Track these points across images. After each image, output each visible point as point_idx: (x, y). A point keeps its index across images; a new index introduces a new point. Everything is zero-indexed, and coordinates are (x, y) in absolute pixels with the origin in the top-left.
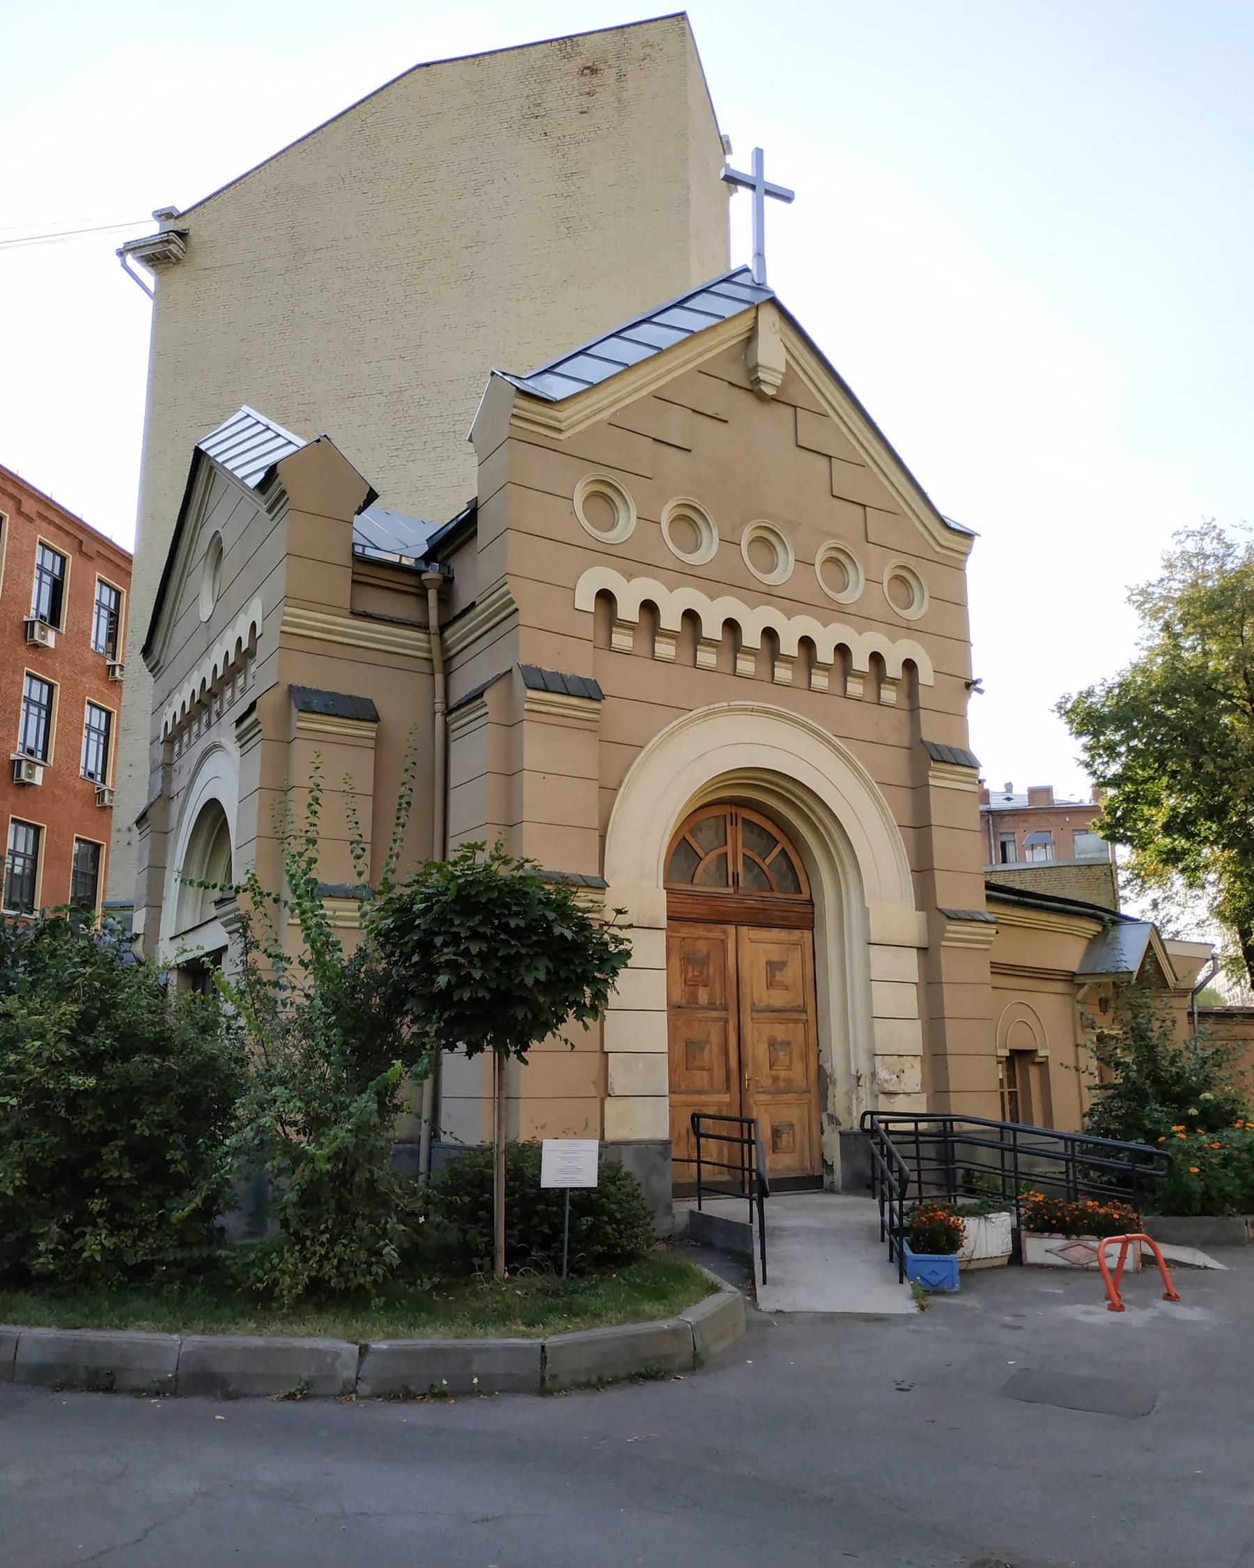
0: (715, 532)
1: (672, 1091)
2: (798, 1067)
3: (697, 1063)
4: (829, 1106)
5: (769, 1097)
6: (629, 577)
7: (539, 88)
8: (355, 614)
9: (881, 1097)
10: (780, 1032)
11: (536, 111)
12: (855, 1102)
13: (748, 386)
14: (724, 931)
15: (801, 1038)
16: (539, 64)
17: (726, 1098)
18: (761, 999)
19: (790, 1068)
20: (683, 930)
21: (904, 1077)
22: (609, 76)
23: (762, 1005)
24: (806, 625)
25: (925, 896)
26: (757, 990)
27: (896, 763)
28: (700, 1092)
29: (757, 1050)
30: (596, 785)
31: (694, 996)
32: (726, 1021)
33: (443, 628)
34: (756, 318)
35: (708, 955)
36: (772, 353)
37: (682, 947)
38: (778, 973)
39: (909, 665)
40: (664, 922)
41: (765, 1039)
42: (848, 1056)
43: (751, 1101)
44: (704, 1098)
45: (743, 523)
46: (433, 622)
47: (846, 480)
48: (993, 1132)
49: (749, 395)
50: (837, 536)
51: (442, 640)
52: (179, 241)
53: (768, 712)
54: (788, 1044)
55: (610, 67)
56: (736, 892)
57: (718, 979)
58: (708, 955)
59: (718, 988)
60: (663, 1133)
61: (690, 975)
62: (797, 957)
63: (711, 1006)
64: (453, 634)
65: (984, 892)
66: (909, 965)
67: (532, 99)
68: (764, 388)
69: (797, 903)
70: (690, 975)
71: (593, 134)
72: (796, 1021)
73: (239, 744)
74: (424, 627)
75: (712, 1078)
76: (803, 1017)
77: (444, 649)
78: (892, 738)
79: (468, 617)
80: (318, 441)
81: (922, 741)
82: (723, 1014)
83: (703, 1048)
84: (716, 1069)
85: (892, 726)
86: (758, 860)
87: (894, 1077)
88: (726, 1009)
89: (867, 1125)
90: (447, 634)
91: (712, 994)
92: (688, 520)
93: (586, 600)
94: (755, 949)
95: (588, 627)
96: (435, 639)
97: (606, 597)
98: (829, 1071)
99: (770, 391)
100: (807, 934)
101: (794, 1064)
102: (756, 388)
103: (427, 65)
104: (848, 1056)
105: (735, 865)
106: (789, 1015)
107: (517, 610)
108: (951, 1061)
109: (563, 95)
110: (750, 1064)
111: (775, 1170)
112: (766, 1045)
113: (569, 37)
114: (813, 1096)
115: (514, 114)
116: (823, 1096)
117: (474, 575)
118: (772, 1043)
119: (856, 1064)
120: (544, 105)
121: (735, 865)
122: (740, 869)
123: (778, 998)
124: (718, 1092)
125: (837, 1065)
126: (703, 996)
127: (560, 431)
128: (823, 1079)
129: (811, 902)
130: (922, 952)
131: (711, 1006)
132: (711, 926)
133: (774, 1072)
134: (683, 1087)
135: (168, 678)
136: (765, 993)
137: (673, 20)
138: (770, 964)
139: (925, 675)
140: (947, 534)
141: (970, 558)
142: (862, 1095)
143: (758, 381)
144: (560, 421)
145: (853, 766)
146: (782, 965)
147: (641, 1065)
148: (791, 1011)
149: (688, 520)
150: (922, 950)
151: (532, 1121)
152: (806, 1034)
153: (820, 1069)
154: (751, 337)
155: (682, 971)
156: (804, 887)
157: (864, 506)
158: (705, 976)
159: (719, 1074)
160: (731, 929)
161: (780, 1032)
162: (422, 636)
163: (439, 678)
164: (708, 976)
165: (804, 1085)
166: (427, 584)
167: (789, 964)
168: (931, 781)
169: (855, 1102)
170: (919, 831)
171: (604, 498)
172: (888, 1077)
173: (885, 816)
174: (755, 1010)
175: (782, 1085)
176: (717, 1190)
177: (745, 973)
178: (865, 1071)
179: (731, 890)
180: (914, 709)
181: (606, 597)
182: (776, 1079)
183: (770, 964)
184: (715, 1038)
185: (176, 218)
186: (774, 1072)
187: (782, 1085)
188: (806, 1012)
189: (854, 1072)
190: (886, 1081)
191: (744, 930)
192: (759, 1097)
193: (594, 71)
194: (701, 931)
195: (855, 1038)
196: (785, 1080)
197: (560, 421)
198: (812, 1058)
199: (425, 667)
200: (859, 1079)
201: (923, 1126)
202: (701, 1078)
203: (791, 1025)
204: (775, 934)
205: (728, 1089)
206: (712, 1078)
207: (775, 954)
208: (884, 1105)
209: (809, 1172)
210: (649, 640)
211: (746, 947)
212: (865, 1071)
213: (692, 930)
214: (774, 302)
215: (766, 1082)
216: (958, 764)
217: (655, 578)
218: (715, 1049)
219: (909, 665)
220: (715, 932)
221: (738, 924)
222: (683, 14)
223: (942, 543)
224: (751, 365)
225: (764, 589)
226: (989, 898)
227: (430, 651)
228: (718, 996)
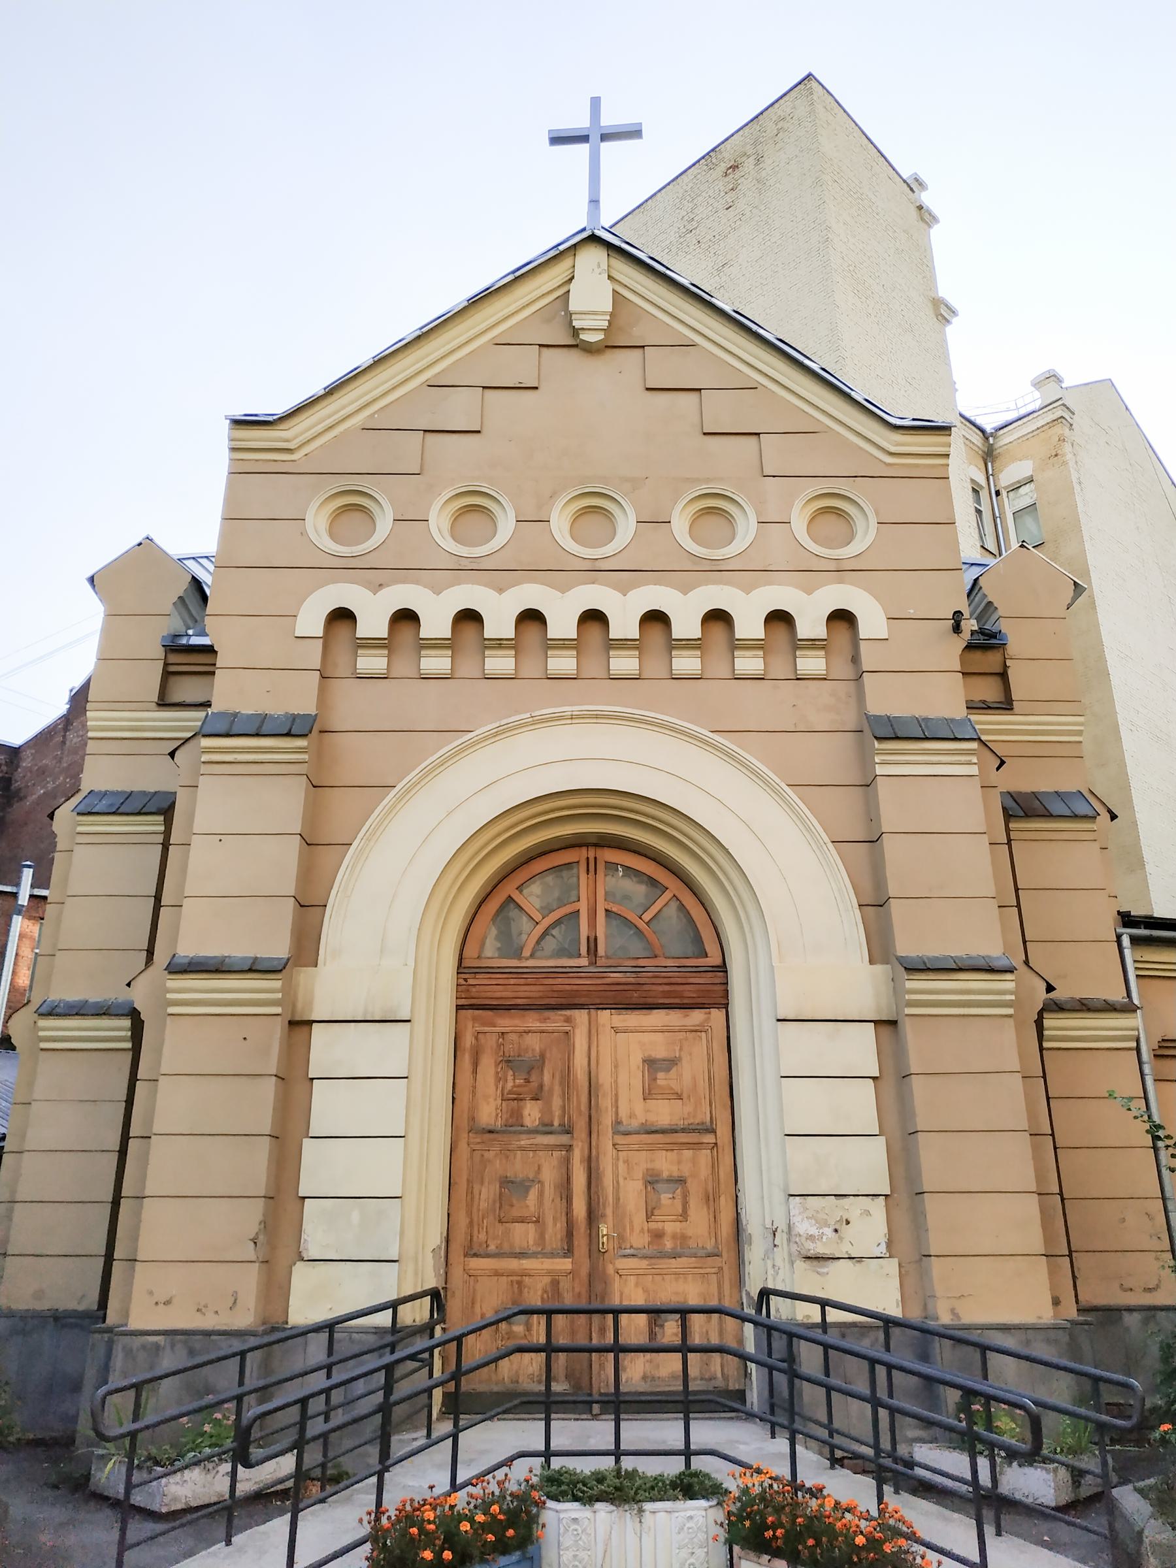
2: (699, 1218)
3: (515, 1212)
5: (644, 1263)
9: (800, 1265)
10: (666, 1163)
12: (771, 1271)
14: (568, 1020)
15: (704, 1171)
17: (566, 1264)
18: (632, 1116)
19: (684, 1216)
20: (500, 1021)
22: (749, 164)
23: (635, 1124)
26: (627, 1100)
27: (830, 756)
28: (522, 1255)
29: (625, 1187)
30: (994, 904)
31: (517, 1115)
32: (569, 1148)
35: (543, 1056)
37: (499, 1046)
38: (661, 1075)
41: (639, 1173)
43: (610, 1270)
44: (526, 1264)
47: (722, 411)
48: (870, 1327)
49: (574, 351)
50: (697, 481)
53: (597, 716)
54: (681, 1181)
55: (749, 157)
56: (593, 963)
57: (557, 1090)
58: (543, 1056)
59: (557, 1102)
61: (510, 1084)
63: (546, 1128)
68: (584, 336)
69: (698, 971)
70: (510, 1084)
71: (738, 223)
72: (697, 1146)
75: (542, 1236)
76: (709, 1139)
78: (821, 721)
80: (140, 544)
82: (564, 1139)
83: (527, 1190)
84: (549, 1221)
85: (824, 706)
87: (828, 1232)
91: (547, 1110)
94: (620, 1049)
100: (717, 1015)
101: (692, 1212)
106: (682, 1138)
110: (609, 1211)
111: (653, 1379)
112: (639, 1185)
113: (712, 150)
118: (652, 1181)
123: (664, 1113)
124: (552, 1255)
126: (532, 1113)
130: (886, 1031)
131: (546, 1128)
132: (547, 1013)
133: (653, 1225)
134: (492, 1248)
136: (639, 1106)
137: (801, 86)
138: (651, 1064)
140: (897, 437)
142: (779, 1262)
143: (575, 332)
144: (287, 441)
145: (753, 772)
146: (672, 1063)
147: (355, 1216)
148: (683, 1130)
149: (474, 509)
151: (151, 1293)
152: (715, 1165)
155: (498, 1080)
156: (711, 947)
157: (758, 434)
158: (534, 1085)
159: (555, 1231)
160: (581, 1016)
161: (666, 1163)
164: (541, 1086)
167: (685, 1063)
168: (879, 770)
169: (771, 1271)
171: (353, 508)
172: (813, 1231)
173: (809, 830)
174: (618, 1128)
175: (668, 1245)
176: (726, 1403)
177: (605, 1077)
178: (781, 1225)
179: (584, 962)
182: (658, 1236)
183: (651, 1064)
184: (550, 1175)
186: (653, 1225)
187: (668, 1245)
188: (712, 1130)
189: (769, 1225)
190: (811, 1238)
191: (604, 1016)
192: (622, 1263)
193: (734, 167)
194: (532, 1021)
196: (674, 1237)
197: (287, 441)
198: (725, 1204)
201: (834, 1315)
202: (524, 1235)
203: (688, 1154)
204: (658, 1018)
205: (569, 1252)
206: (542, 1236)
207: (659, 1047)
209: (720, 1383)
211: (606, 1040)
212: (781, 1225)
213: (517, 1022)
215: (638, 1239)
216: (927, 739)
217: (417, 582)
218: (549, 1192)
220: (556, 1021)
223: (893, 449)
228: (557, 1113)
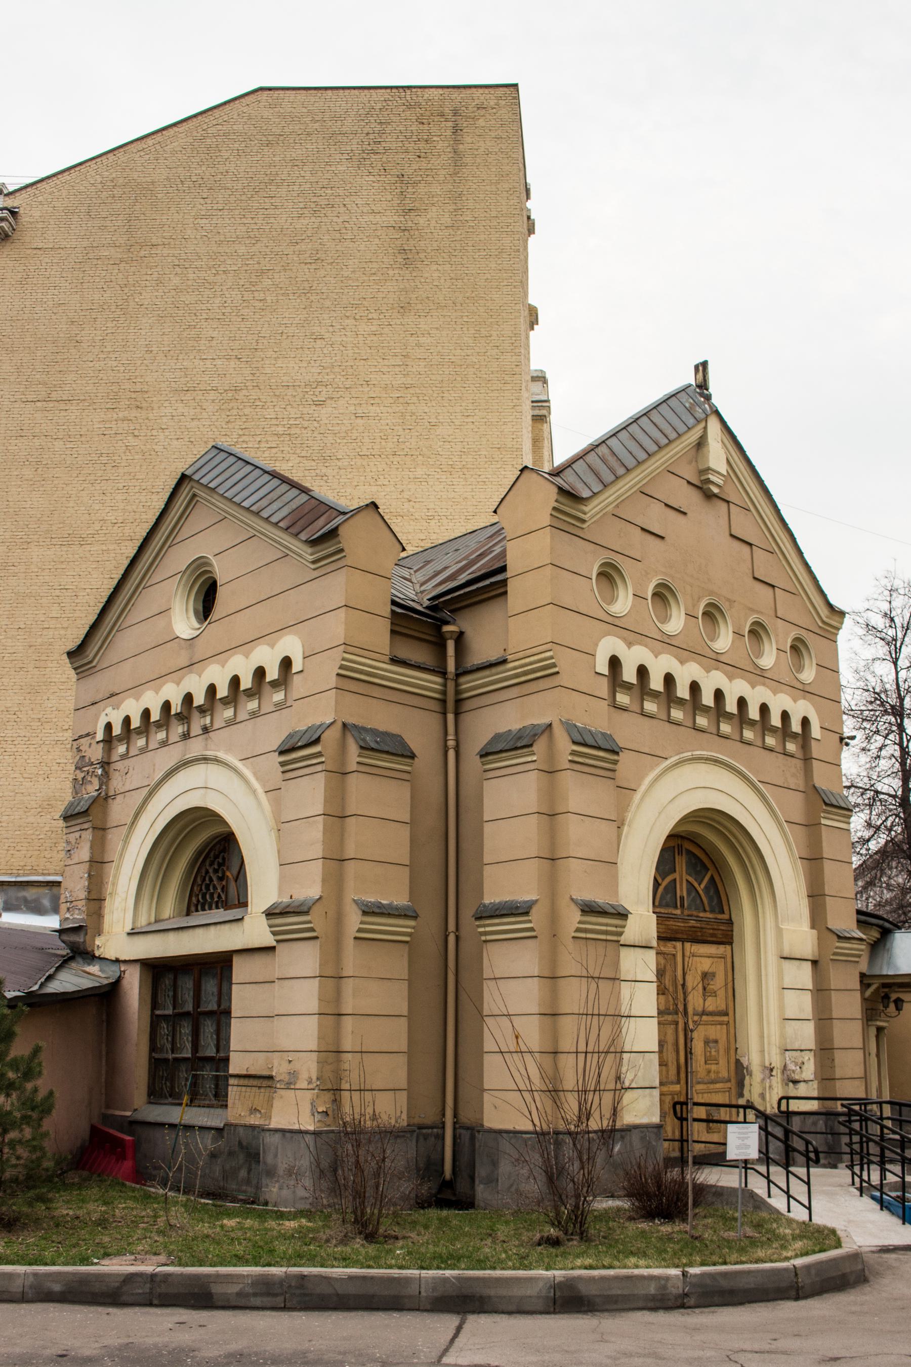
0: (682, 609)
1: (661, 1084)
4: (746, 1092)
6: (630, 644)
7: (378, 128)
8: (395, 661)
9: (791, 1084)
11: (375, 147)
13: (699, 484)
14: (675, 947)
16: (379, 106)
17: (677, 1088)
21: (804, 1067)
24: (686, 673)
25: (817, 917)
32: (677, 1023)
33: (458, 675)
34: (705, 428)
35: (665, 967)
36: (717, 457)
39: (805, 722)
40: (654, 943)
42: (762, 1051)
45: (699, 599)
46: (451, 667)
50: (758, 612)
51: (457, 685)
52: (11, 219)
54: (716, 1042)
58: (665, 967)
60: (656, 1119)
62: (722, 967)
64: (467, 682)
65: (854, 916)
66: (804, 975)
67: (371, 136)
72: (721, 1023)
73: (282, 769)
74: (443, 674)
76: (725, 1019)
77: (458, 692)
79: (494, 670)
81: (814, 786)
86: (696, 885)
88: (677, 1014)
89: (784, 1108)
90: (462, 680)
92: (663, 595)
93: (603, 667)
94: (702, 958)
95: (603, 689)
96: (451, 685)
97: (615, 663)
98: (745, 1064)
99: (716, 490)
100: (728, 947)
102: (705, 487)
103: (270, 89)
104: (762, 1051)
105: (681, 890)
107: (558, 673)
108: (838, 1055)
109: (401, 138)
114: (733, 1084)
115: (354, 147)
116: (741, 1084)
117: (487, 634)
119: (770, 1059)
120: (384, 144)
121: (681, 890)
122: (685, 894)
124: (672, 1083)
125: (753, 1059)
127: (584, 521)
128: (740, 1072)
129: (730, 922)
135: (100, 683)
139: (816, 731)
141: (841, 631)
150: (815, 963)
153: (738, 1063)
154: (701, 444)
156: (726, 908)
160: (679, 945)
162: (439, 680)
163: (451, 717)
165: (726, 1075)
166: (448, 635)
170: (813, 861)
172: (794, 1068)
178: (777, 1062)
180: (807, 759)
181: (615, 663)
185: (5, 195)
187: (713, 1076)
189: (767, 1064)
190: (794, 1072)
191: (688, 945)
195: (769, 1037)
198: (732, 1052)
199: (435, 706)
200: (772, 1070)
203: (719, 1027)
205: (678, 1082)
207: (705, 965)
208: (792, 1091)
210: (691, 712)
214: (717, 413)
217: (646, 646)
219: (805, 722)
221: (683, 941)
222: (516, 86)
224: (701, 467)
225: (714, 656)
226: (858, 921)
227: (444, 693)
